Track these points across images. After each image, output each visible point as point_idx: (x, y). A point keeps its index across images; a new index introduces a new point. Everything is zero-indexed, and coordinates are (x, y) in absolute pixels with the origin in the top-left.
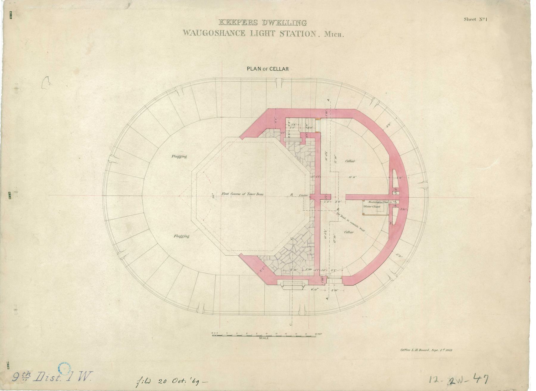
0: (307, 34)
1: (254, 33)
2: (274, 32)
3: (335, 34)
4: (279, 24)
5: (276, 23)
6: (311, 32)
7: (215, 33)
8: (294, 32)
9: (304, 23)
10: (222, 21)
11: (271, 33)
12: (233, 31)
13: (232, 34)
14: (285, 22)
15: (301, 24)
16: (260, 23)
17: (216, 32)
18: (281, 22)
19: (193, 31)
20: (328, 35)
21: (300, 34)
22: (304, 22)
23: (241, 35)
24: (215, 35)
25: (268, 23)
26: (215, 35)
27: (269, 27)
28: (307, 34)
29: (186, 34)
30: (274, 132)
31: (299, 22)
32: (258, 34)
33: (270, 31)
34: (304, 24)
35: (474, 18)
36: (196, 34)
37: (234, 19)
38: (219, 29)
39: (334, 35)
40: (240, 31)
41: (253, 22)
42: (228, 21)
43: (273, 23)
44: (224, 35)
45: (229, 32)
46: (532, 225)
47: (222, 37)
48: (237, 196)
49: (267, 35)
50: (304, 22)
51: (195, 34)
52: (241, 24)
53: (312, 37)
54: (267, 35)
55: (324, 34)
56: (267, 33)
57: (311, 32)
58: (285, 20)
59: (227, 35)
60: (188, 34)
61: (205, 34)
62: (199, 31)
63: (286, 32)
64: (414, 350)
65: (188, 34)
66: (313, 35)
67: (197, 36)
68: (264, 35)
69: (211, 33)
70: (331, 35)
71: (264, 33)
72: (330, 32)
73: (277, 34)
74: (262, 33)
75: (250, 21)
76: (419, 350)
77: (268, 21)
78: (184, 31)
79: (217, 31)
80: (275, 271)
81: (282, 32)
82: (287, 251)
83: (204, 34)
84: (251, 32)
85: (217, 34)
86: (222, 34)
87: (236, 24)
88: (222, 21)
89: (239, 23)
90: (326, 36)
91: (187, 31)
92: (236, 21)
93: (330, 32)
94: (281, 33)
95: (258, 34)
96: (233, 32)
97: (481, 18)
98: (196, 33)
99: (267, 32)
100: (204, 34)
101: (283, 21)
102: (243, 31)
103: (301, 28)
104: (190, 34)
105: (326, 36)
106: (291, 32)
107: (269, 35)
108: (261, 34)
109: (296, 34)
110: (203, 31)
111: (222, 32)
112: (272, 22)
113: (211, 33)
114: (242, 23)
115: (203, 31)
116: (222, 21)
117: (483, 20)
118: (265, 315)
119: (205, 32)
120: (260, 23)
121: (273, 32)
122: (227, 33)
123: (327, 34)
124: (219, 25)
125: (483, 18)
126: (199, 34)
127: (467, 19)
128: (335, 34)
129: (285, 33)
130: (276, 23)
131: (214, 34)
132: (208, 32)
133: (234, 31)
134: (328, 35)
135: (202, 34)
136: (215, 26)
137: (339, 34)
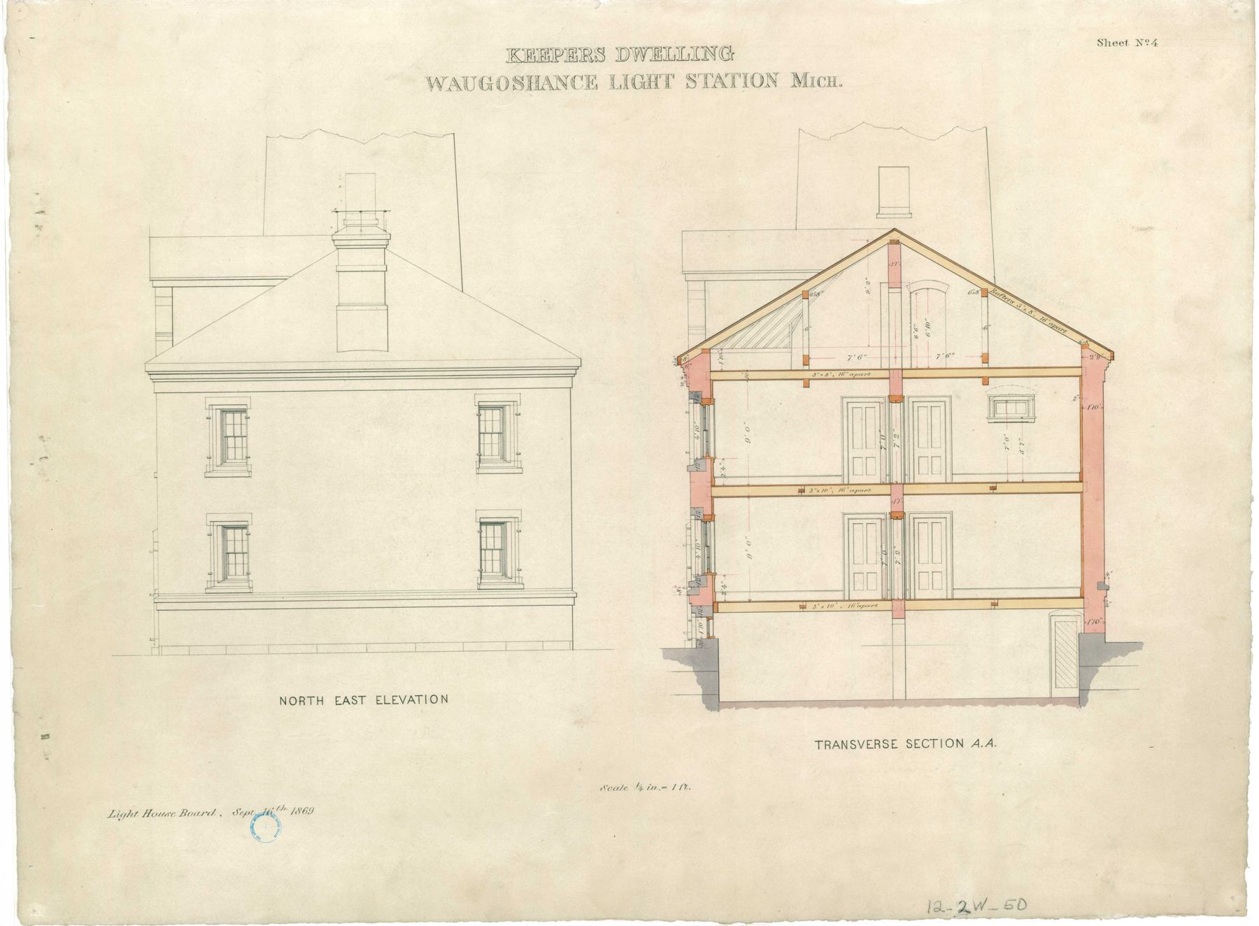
0: (757, 82)
1: (619, 81)
4: (657, 57)
5: (650, 54)
7: (511, 83)
9: (728, 53)
10: (513, 52)
11: (662, 82)
12: (564, 79)
13: (560, 86)
16: (611, 54)
19: (454, 80)
21: (739, 82)
23: (585, 87)
26: (514, 88)
29: (436, 87)
32: (630, 85)
34: (726, 57)
35: (1124, 41)
36: (462, 87)
37: (516, 47)
40: (584, 78)
41: (593, 56)
42: (530, 55)
44: (540, 88)
45: (554, 82)
46: (632, 922)
47: (534, 93)
49: (653, 84)
51: (551, 86)
52: (565, 57)
54: (653, 84)
58: (673, 46)
59: (546, 87)
60: (440, 87)
61: (485, 87)
62: (470, 80)
63: (730, 76)
65: (440, 87)
66: (771, 83)
67: (464, 91)
69: (503, 83)
70: (809, 83)
71: (646, 79)
72: (805, 75)
73: (679, 83)
74: (638, 80)
82: (715, 380)
85: (518, 87)
87: (664, 58)
88: (514, 51)
90: (797, 85)
92: (579, 51)
94: (690, 78)
95: (630, 85)
98: (462, 85)
99: (653, 78)
100: (482, 88)
101: (680, 49)
103: (717, 67)
105: (797, 85)
107: (656, 85)
109: (728, 81)
111: (533, 80)
112: (640, 53)
113: (503, 83)
114: (565, 57)
116: (513, 52)
117: (1144, 43)
118: (483, 551)
120: (611, 54)
121: (706, 78)
122: (453, 83)
126: (470, 86)
127: (1104, 42)
129: (700, 80)
130: (650, 54)
131: (511, 87)
132: (494, 80)
135: (477, 87)
136: (501, 68)
137: (829, 78)
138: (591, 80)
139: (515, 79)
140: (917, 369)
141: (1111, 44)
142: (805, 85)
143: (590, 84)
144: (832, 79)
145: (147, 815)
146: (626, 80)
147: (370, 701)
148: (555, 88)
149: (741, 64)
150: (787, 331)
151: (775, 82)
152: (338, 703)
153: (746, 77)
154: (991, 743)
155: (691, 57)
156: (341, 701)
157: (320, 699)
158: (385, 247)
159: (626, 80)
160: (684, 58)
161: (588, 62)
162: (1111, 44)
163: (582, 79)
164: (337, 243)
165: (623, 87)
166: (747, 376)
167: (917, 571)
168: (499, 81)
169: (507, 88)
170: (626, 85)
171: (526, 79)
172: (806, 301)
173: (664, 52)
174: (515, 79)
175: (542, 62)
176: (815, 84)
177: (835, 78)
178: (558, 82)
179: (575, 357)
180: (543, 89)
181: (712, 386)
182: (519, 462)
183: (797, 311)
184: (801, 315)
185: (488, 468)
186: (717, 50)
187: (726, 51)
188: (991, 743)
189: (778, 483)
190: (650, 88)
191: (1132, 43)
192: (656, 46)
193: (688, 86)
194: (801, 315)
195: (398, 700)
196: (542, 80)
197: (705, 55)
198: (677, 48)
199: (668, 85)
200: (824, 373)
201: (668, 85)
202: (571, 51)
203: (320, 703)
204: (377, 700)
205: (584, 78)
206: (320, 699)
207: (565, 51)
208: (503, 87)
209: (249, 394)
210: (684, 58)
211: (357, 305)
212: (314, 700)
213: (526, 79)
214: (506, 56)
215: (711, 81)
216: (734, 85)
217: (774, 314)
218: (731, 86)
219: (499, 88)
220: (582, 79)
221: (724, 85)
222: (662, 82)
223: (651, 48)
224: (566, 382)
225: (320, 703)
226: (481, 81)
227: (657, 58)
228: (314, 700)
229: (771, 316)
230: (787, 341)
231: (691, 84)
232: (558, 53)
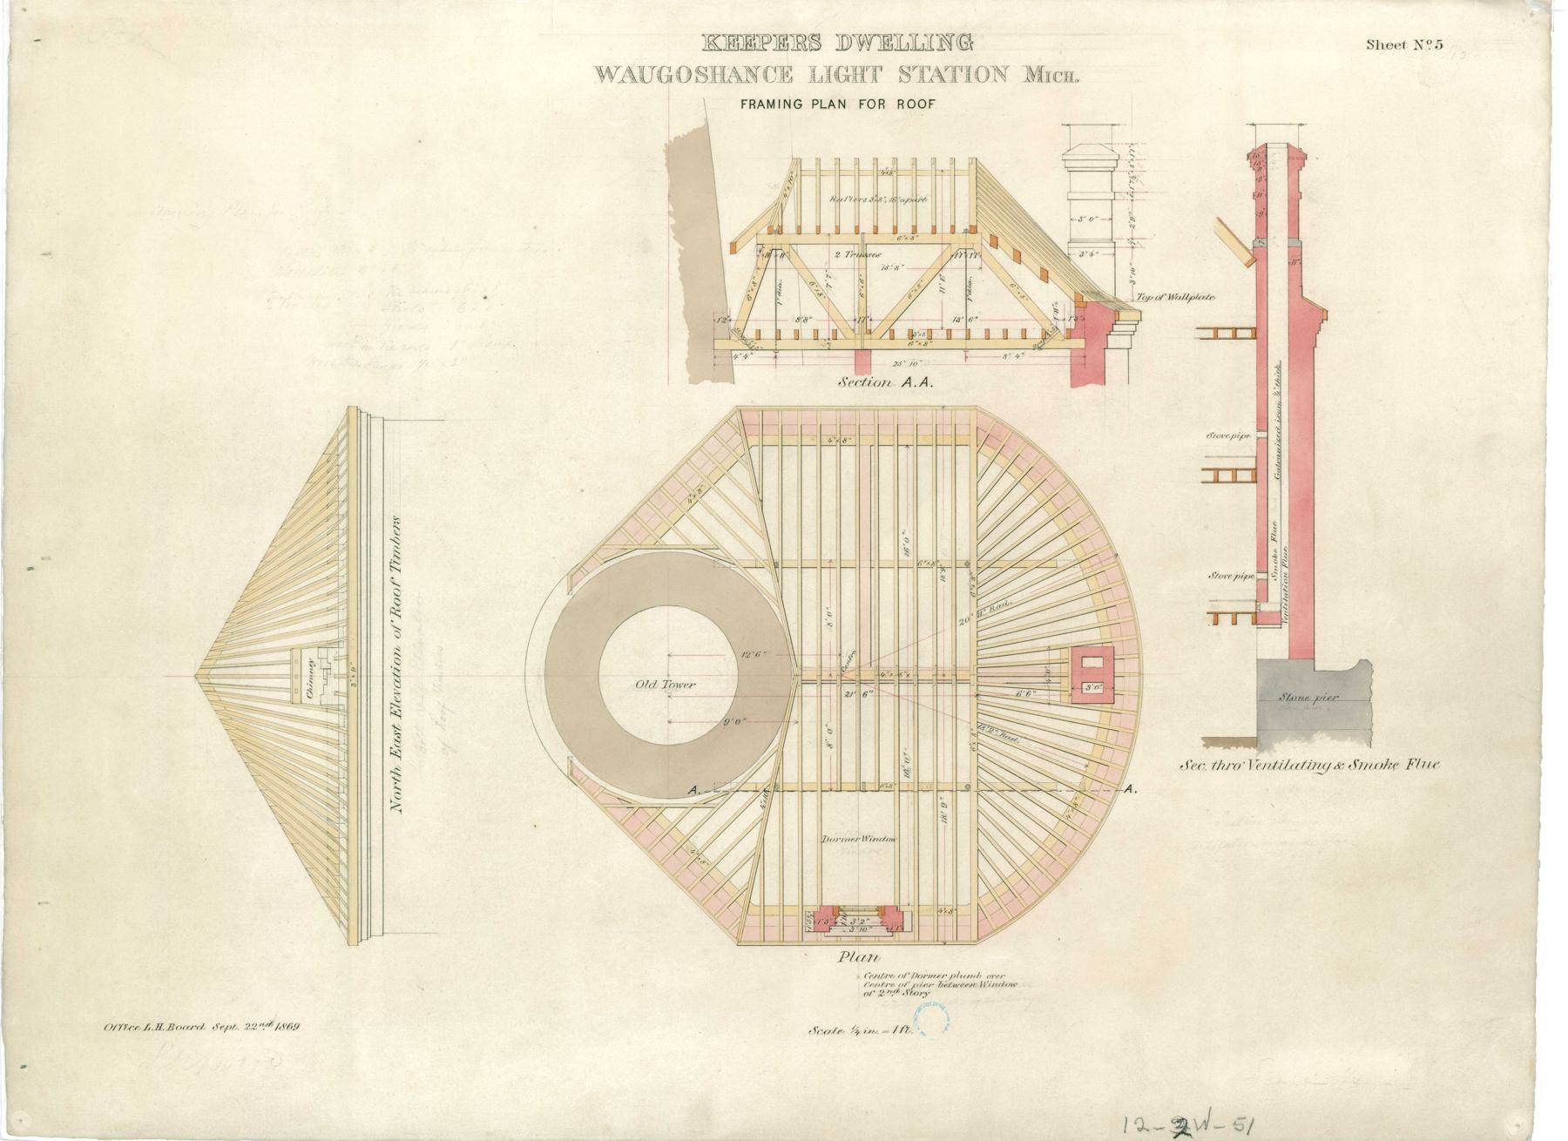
1: (821, 72)
2: (878, 69)
5: (876, 42)
6: (992, 71)
8: (942, 70)
11: (868, 75)
13: (750, 79)
15: (954, 43)
16: (830, 43)
19: (629, 70)
20: (1036, 78)
21: (961, 76)
22: (965, 39)
23: (779, 79)
24: (697, 81)
25: (855, 46)
26: (697, 81)
27: (855, 57)
29: (607, 77)
31: (946, 41)
32: (832, 78)
35: (1401, 42)
36: (638, 79)
40: (778, 70)
41: (807, 43)
44: (726, 80)
45: (743, 73)
49: (859, 78)
52: (773, 45)
57: (992, 71)
58: (906, 33)
59: (734, 80)
61: (664, 79)
63: (918, 70)
64: (153, 1026)
68: (851, 78)
70: (1044, 78)
71: (850, 72)
72: (1040, 69)
74: (842, 72)
76: (165, 1026)
77: (853, 38)
79: (702, 70)
80: (1114, 694)
81: (904, 68)
83: (660, 78)
84: (809, 70)
85: (701, 79)
86: (718, 78)
88: (711, 38)
89: (765, 46)
94: (903, 72)
95: (832, 78)
97: (1420, 42)
99: (859, 71)
100: (660, 78)
101: (899, 36)
103: (956, 57)
104: (618, 78)
106: (933, 69)
109: (948, 76)
110: (660, 71)
111: (718, 71)
112: (864, 42)
114: (773, 45)
115: (660, 71)
119: (665, 72)
120: (830, 43)
122: (936, 74)
125: (1425, 42)
127: (1375, 44)
129: (915, 74)
130: (876, 42)
132: (673, 73)
133: (757, 68)
134: (1036, 78)
135: (655, 78)
138: (785, 71)
139: (997, 69)
141: (1385, 47)
142: (1040, 79)
145: (397, 613)
149: (978, 57)
153: (969, 71)
154: (925, 382)
155: (910, 47)
160: (902, 48)
161: (802, 51)
163: (775, 71)
165: (825, 79)
171: (709, 70)
173: (894, 41)
174: (698, 71)
176: (1051, 79)
178: (997, 74)
186: (954, 39)
187: (965, 39)
188: (925, 382)
189: (996, 351)
190: (856, 81)
191: (1411, 45)
192: (781, 33)
196: (728, 72)
197: (942, 45)
198: (925, 35)
199: (875, 78)
201: (875, 78)
202: (731, 38)
205: (778, 70)
207: (774, 38)
210: (902, 48)
214: (702, 43)
215: (928, 76)
216: (954, 80)
218: (964, 80)
219: (679, 79)
220: (775, 71)
221: (942, 80)
223: (724, 35)
227: (782, 47)
231: (905, 78)
232: (766, 40)
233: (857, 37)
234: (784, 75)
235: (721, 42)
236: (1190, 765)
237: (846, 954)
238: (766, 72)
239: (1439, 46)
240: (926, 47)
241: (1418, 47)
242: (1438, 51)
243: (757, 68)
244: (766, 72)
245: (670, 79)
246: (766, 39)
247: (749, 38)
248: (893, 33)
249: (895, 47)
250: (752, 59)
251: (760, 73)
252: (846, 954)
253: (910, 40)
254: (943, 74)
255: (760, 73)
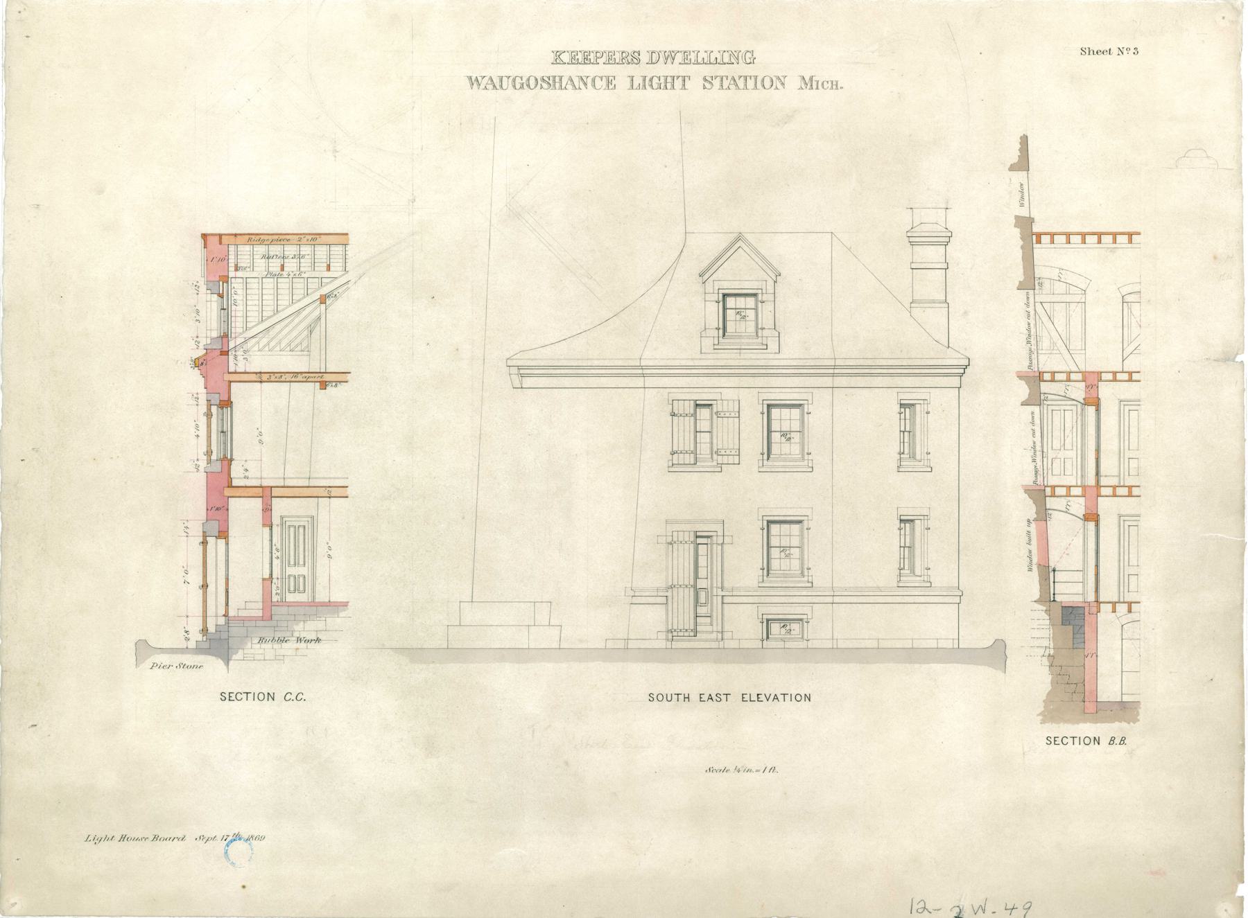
0: (767, 84)
2: (687, 79)
3: (823, 84)
5: (679, 57)
6: (774, 79)
8: (737, 78)
10: (558, 54)
11: (678, 83)
13: (582, 86)
14: (701, 55)
17: (543, 80)
18: (693, 56)
20: (809, 86)
21: (751, 83)
22: (749, 55)
23: (604, 86)
28: (767, 84)
30: (1042, 349)
31: (735, 57)
33: (675, 78)
34: (748, 61)
38: (551, 74)
39: (820, 84)
40: (604, 79)
43: (673, 59)
45: (576, 81)
48: (199, 662)
49: (669, 86)
50: (749, 55)
51: (494, 86)
53: (777, 90)
54: (669, 86)
55: (798, 83)
56: (667, 83)
59: (569, 87)
61: (518, 86)
62: (505, 79)
66: (779, 86)
69: (532, 82)
70: (814, 86)
71: (662, 80)
72: (811, 79)
73: (695, 84)
74: (655, 80)
75: (624, 55)
78: (470, 78)
82: (233, 382)
83: (514, 87)
84: (629, 79)
85: (545, 85)
88: (558, 54)
90: (803, 87)
91: (477, 80)
92: (592, 54)
93: (811, 79)
96: (585, 80)
97: (1122, 49)
100: (514, 87)
101: (709, 52)
102: (610, 78)
103: (741, 69)
106: (730, 78)
108: (655, 86)
109: (741, 83)
112: (670, 56)
113: (532, 82)
116: (558, 54)
117: (1125, 52)
119: (518, 80)
122: (490, 82)
123: (806, 84)
124: (552, 64)
125: (1125, 49)
128: (823, 84)
129: (717, 82)
130: (679, 57)
132: (524, 80)
133: (605, 89)
139: (778, 78)
140: (235, 373)
141: (1095, 53)
143: (610, 84)
144: (834, 83)
146: (644, 80)
147: (735, 699)
148: (577, 87)
150: (306, 333)
151: (783, 84)
152: (744, 699)
155: (718, 61)
156: (705, 697)
157: (686, 696)
158: (946, 243)
159: (644, 80)
162: (1095, 53)
164: (911, 239)
166: (261, 377)
167: (1126, 573)
168: (528, 80)
169: (536, 87)
170: (645, 86)
172: (323, 306)
175: (585, 63)
176: (820, 86)
177: (837, 82)
179: (514, 357)
180: (828, 82)
181: (230, 386)
182: (810, 462)
183: (316, 313)
184: (319, 318)
185: (703, 467)
186: (740, 54)
190: (666, 89)
191: (1114, 51)
193: (704, 88)
194: (319, 318)
195: (762, 698)
198: (706, 52)
200: (283, 379)
203: (687, 700)
204: (743, 698)
206: (686, 696)
207: (604, 54)
208: (532, 86)
209: (928, 390)
211: (925, 303)
212: (681, 697)
213: (551, 78)
214: (552, 57)
215: (726, 84)
217: (292, 318)
218: (681, 87)
222: (678, 83)
223: (568, 52)
224: (955, 381)
225: (687, 700)
226: (514, 80)
228: (681, 697)
229: (290, 319)
230: (305, 344)
231: (708, 85)
233: (663, 53)
234: (609, 82)
235: (565, 58)
236: (711, 769)
237: (155, 665)
238: (593, 81)
239: (1136, 53)
240: (705, 61)
241: (1120, 53)
242: (1134, 56)
243: (605, 89)
244: (593, 81)
245: (522, 87)
246: (599, 54)
247: (558, 54)
248: (691, 50)
249: (693, 61)
250: (588, 70)
251: (589, 81)
252: (155, 665)
253: (705, 55)
254: (737, 80)
255: (589, 81)
